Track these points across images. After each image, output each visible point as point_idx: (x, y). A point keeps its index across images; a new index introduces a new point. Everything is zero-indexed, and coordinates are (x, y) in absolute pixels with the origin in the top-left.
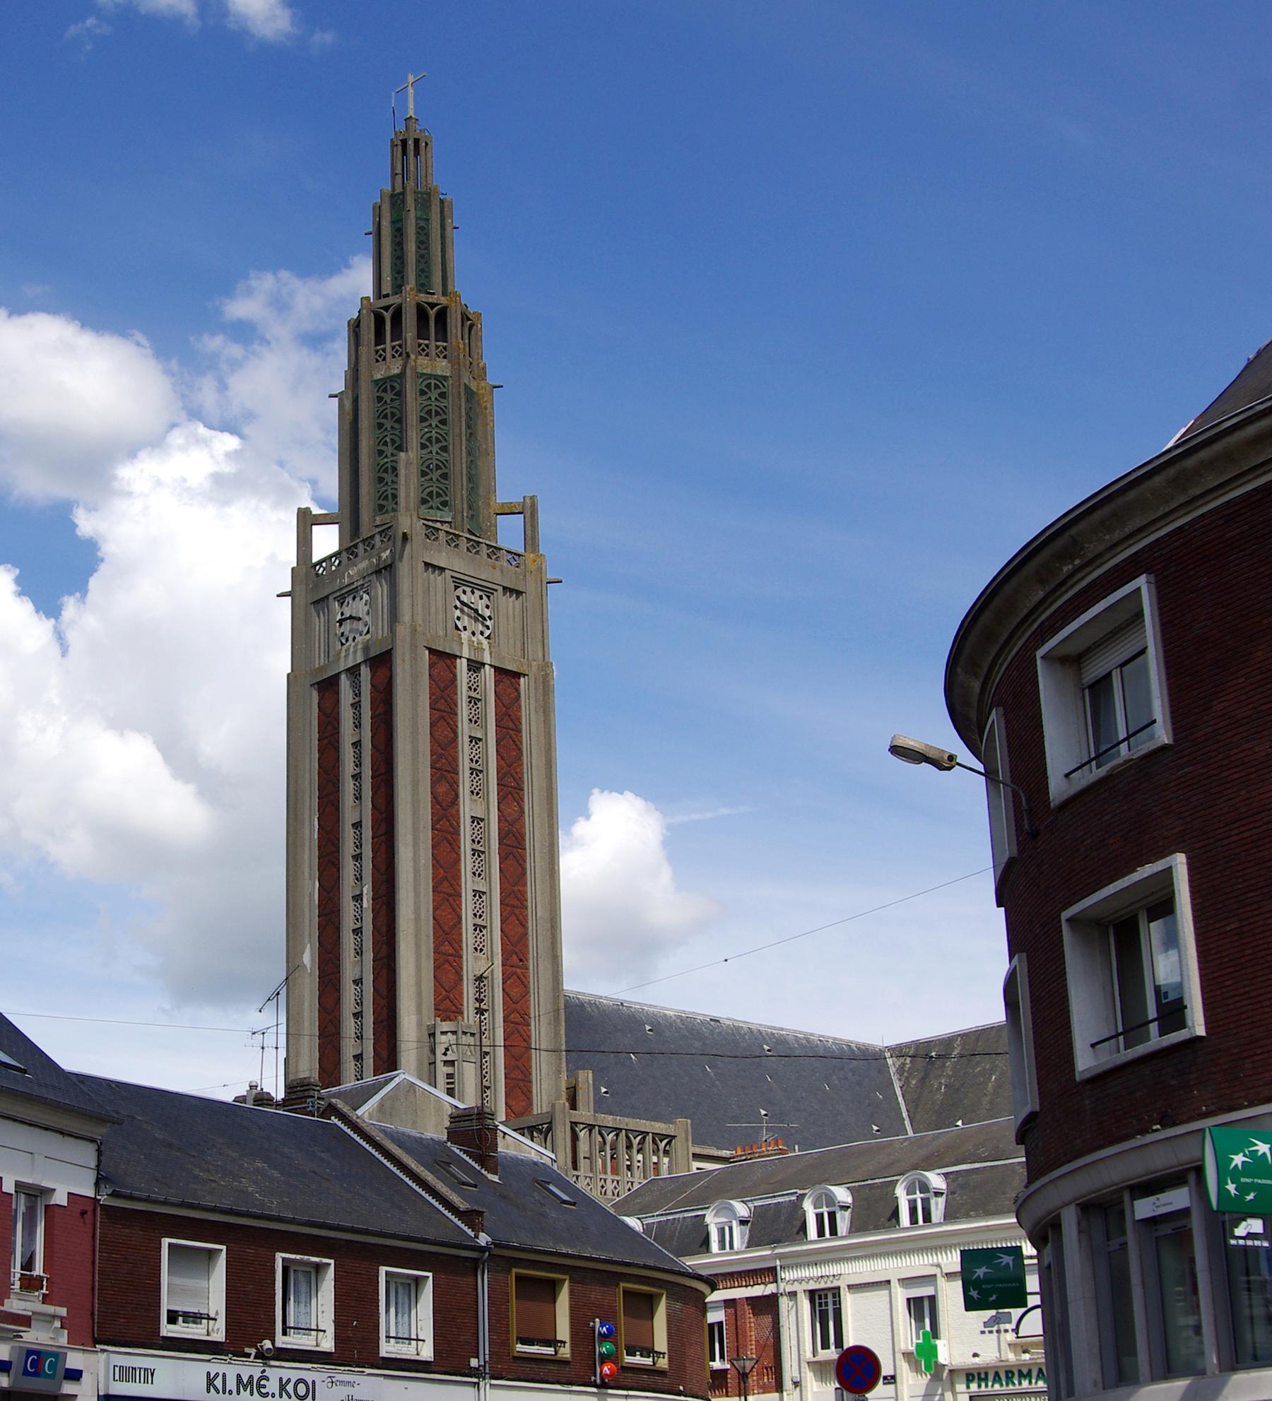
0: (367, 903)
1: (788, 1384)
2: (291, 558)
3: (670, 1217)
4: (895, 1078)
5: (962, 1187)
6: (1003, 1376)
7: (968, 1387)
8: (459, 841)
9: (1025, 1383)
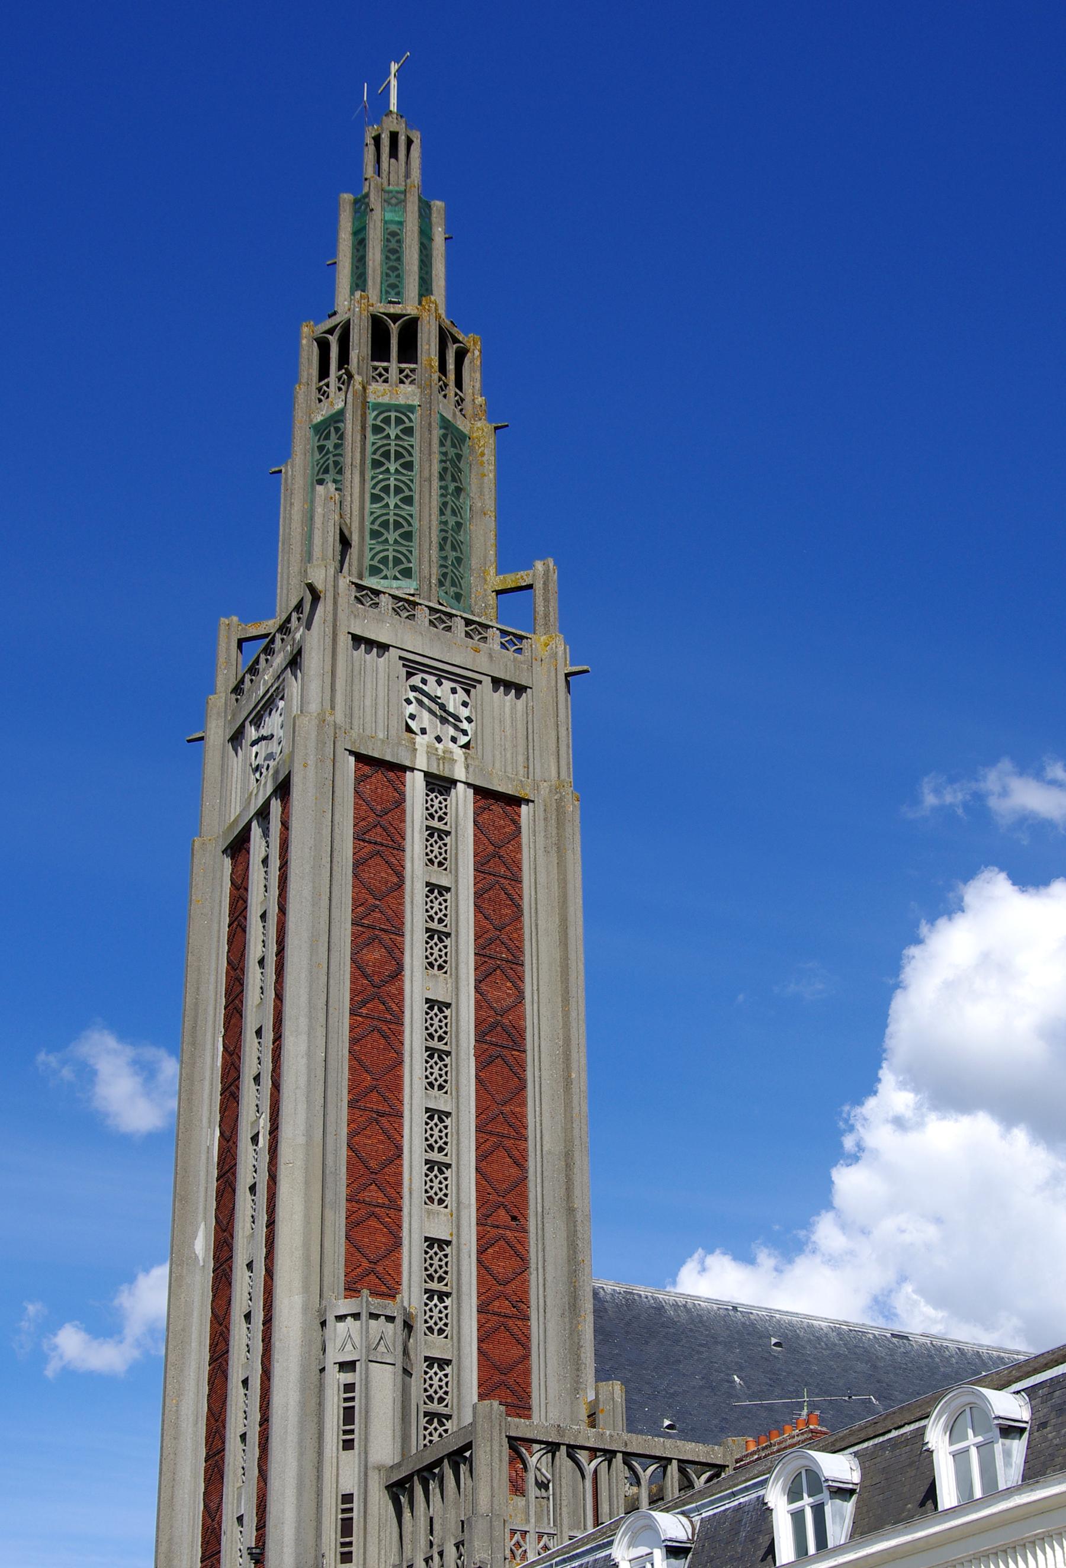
8: (401, 1033)
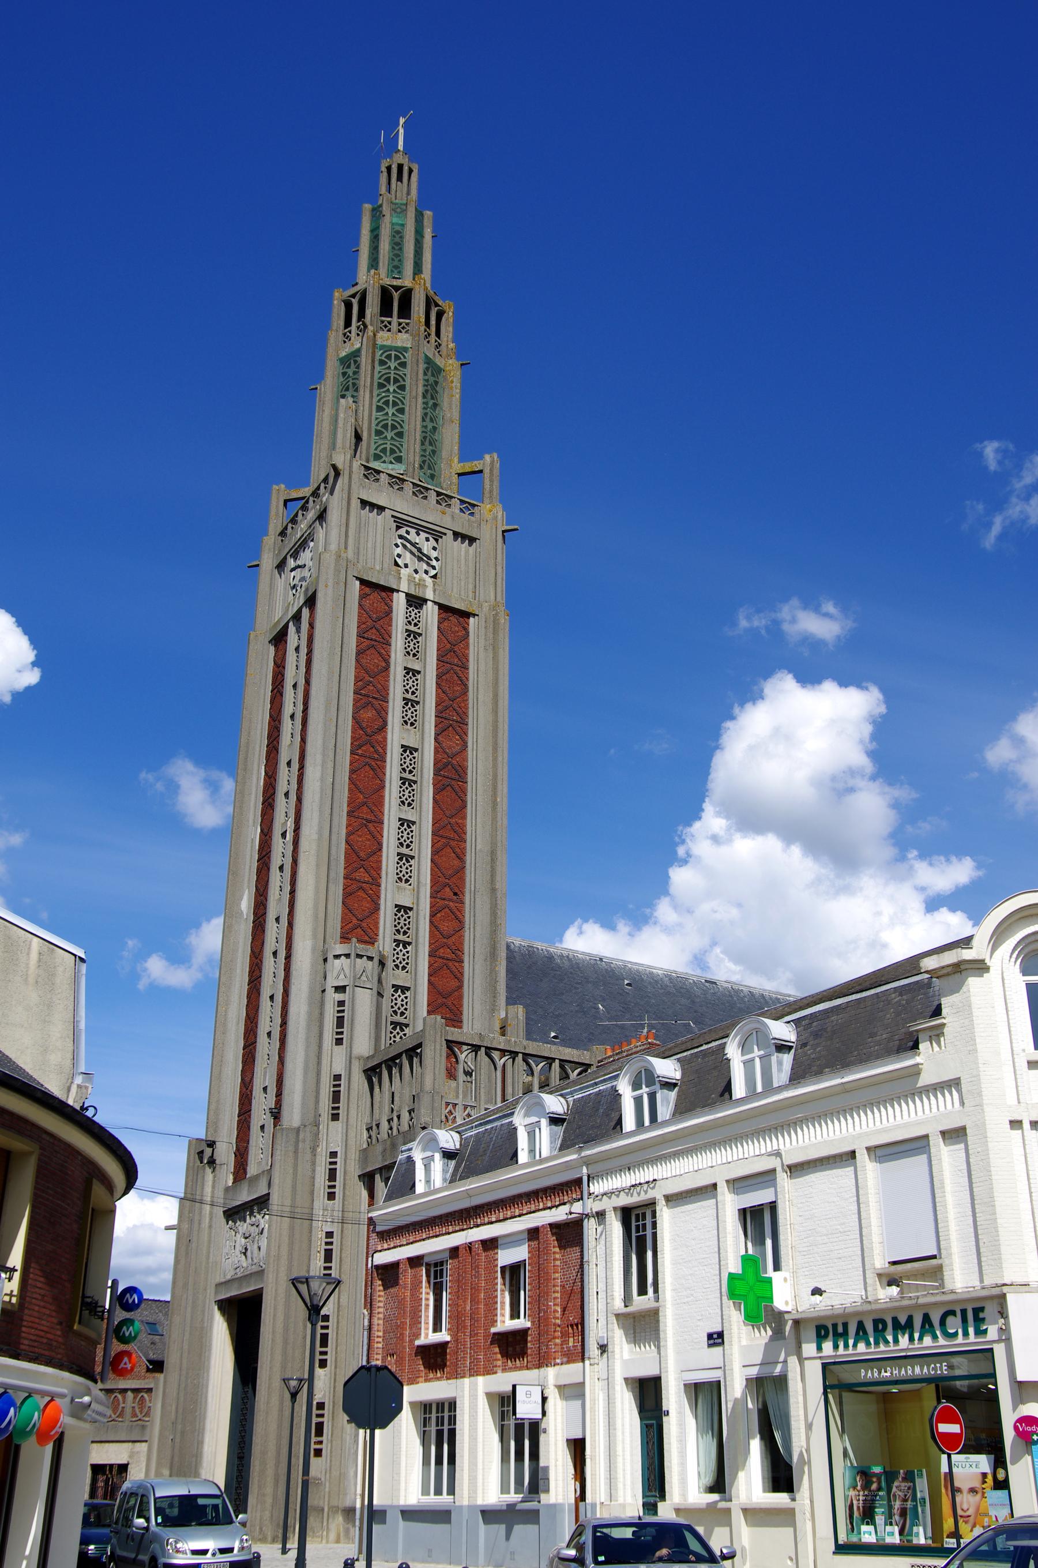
1: (592, 1349)
3: (488, 1127)
5: (816, 1035)
6: (869, 1327)
7: (819, 1349)
8: (384, 767)
9: (904, 1341)
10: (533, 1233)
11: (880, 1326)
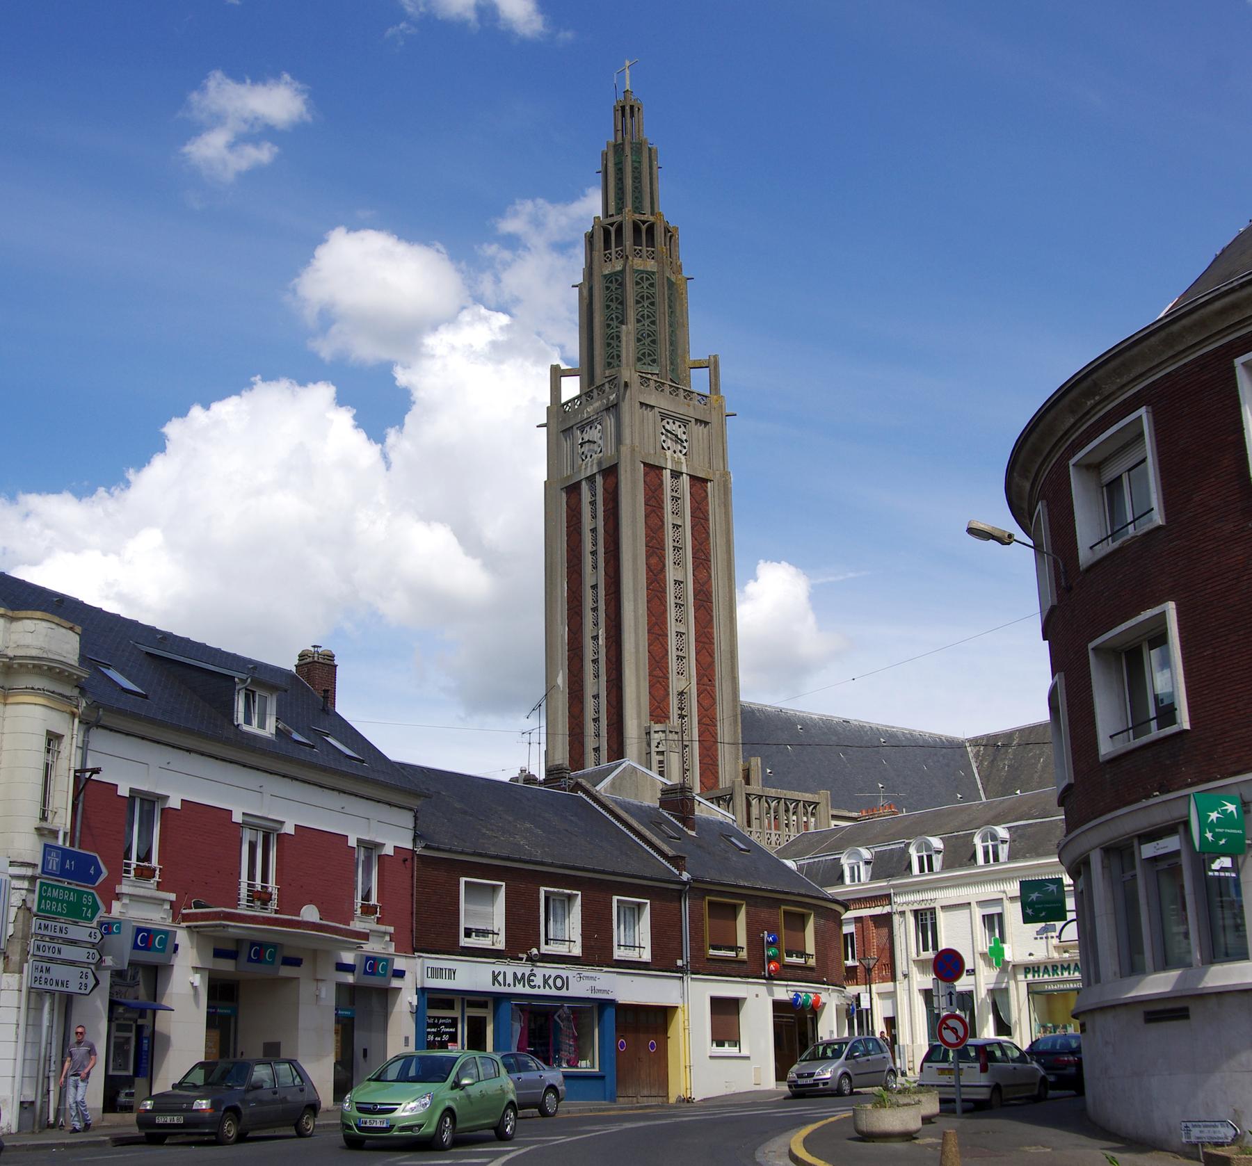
0: (601, 641)
2: (547, 400)
4: (973, 761)
5: (1020, 836)
9: (1066, 974)
10: (858, 920)
11: (1055, 968)
